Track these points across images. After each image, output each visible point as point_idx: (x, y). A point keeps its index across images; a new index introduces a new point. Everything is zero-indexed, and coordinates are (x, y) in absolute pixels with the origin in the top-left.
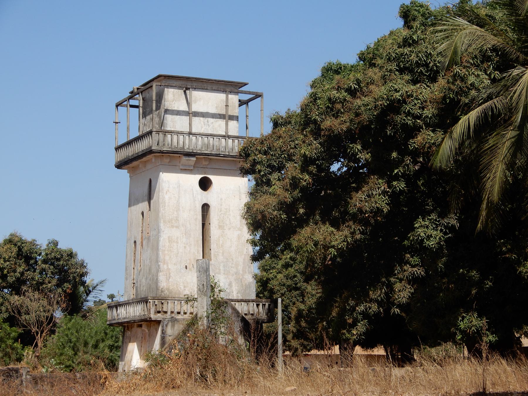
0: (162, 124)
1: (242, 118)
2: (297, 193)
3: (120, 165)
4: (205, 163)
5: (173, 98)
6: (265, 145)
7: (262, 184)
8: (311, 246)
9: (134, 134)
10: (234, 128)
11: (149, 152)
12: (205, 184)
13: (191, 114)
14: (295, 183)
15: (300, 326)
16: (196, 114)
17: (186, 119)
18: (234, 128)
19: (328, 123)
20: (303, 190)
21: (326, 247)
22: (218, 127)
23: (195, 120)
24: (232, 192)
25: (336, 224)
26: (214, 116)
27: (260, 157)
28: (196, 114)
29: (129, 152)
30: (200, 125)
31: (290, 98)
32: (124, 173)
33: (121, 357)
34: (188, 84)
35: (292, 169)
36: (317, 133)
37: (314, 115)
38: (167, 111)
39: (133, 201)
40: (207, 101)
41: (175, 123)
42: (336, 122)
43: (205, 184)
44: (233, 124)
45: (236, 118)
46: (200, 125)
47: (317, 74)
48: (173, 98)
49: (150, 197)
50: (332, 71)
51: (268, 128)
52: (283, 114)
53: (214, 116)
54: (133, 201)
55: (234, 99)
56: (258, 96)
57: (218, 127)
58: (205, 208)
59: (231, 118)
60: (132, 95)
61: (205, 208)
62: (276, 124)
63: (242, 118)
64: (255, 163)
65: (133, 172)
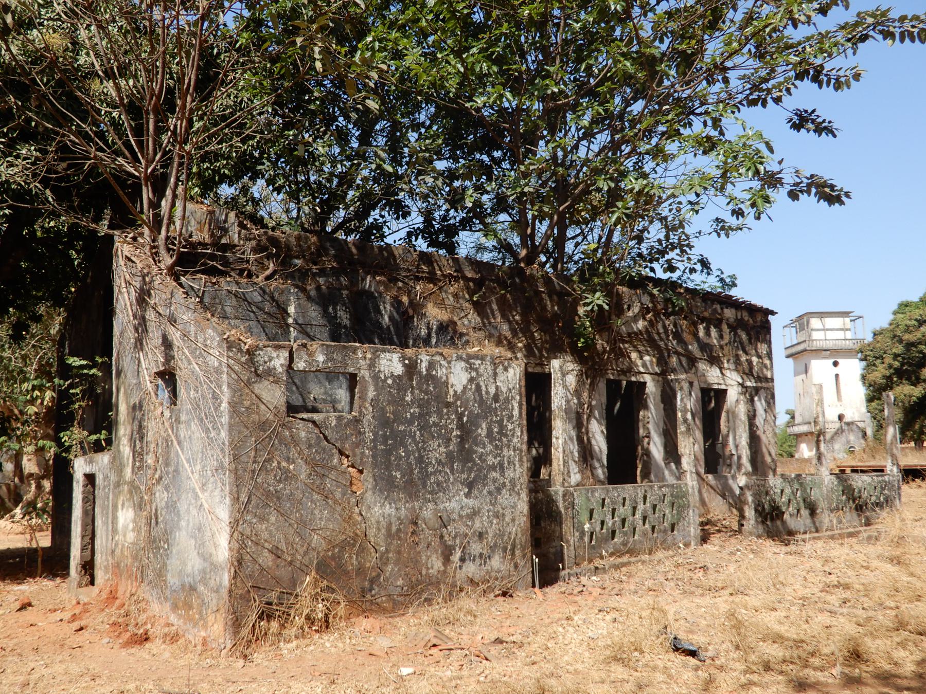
0: (810, 336)
1: (853, 329)
2: (892, 371)
3: (788, 357)
4: (835, 354)
5: (815, 323)
6: (871, 347)
7: (870, 366)
8: (902, 397)
9: (795, 342)
10: (849, 335)
11: (805, 350)
12: (836, 364)
13: (825, 330)
14: (890, 366)
15: (547, 243)
16: (828, 330)
17: (823, 332)
18: (849, 335)
19: (907, 337)
20: (895, 369)
21: (910, 397)
22: (840, 335)
23: (828, 332)
24: (852, 368)
25: (914, 385)
26: (837, 330)
27: (869, 353)
28: (828, 330)
29: (793, 350)
30: (831, 335)
31: (883, 320)
32: (790, 360)
33: (797, 451)
34: (822, 315)
35: (888, 360)
36: (901, 341)
37: (899, 333)
38: (812, 330)
39: (796, 374)
40: (831, 322)
41: (816, 335)
42: (911, 336)
43: (836, 364)
44: (847, 332)
45: (849, 330)
46: (831, 335)
47: (895, 307)
48: (815, 323)
49: (806, 372)
50: (904, 306)
51: (869, 338)
52: (878, 329)
53: (837, 330)
54: (796, 374)
55: (847, 320)
56: (860, 317)
57: (840, 335)
58: (837, 376)
59: (847, 330)
60: (793, 322)
61: (837, 376)
62: (875, 335)
63: (853, 329)
64: (866, 356)
65: (795, 359)
